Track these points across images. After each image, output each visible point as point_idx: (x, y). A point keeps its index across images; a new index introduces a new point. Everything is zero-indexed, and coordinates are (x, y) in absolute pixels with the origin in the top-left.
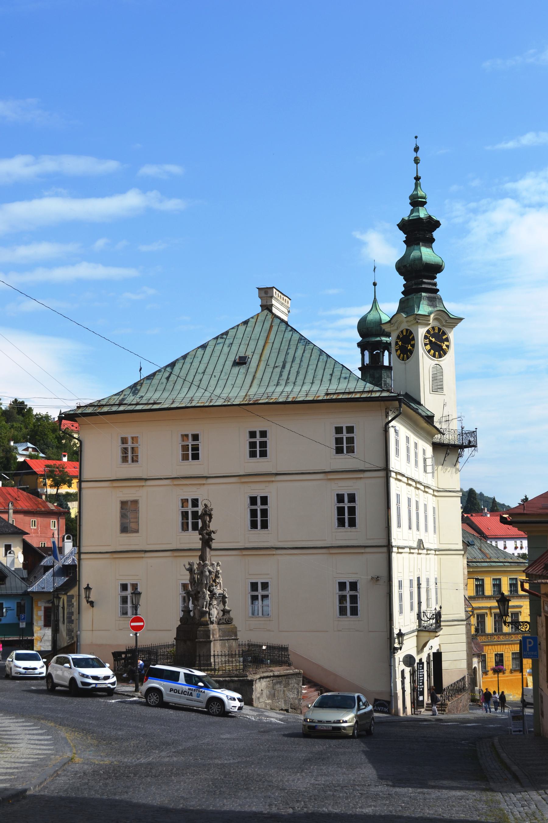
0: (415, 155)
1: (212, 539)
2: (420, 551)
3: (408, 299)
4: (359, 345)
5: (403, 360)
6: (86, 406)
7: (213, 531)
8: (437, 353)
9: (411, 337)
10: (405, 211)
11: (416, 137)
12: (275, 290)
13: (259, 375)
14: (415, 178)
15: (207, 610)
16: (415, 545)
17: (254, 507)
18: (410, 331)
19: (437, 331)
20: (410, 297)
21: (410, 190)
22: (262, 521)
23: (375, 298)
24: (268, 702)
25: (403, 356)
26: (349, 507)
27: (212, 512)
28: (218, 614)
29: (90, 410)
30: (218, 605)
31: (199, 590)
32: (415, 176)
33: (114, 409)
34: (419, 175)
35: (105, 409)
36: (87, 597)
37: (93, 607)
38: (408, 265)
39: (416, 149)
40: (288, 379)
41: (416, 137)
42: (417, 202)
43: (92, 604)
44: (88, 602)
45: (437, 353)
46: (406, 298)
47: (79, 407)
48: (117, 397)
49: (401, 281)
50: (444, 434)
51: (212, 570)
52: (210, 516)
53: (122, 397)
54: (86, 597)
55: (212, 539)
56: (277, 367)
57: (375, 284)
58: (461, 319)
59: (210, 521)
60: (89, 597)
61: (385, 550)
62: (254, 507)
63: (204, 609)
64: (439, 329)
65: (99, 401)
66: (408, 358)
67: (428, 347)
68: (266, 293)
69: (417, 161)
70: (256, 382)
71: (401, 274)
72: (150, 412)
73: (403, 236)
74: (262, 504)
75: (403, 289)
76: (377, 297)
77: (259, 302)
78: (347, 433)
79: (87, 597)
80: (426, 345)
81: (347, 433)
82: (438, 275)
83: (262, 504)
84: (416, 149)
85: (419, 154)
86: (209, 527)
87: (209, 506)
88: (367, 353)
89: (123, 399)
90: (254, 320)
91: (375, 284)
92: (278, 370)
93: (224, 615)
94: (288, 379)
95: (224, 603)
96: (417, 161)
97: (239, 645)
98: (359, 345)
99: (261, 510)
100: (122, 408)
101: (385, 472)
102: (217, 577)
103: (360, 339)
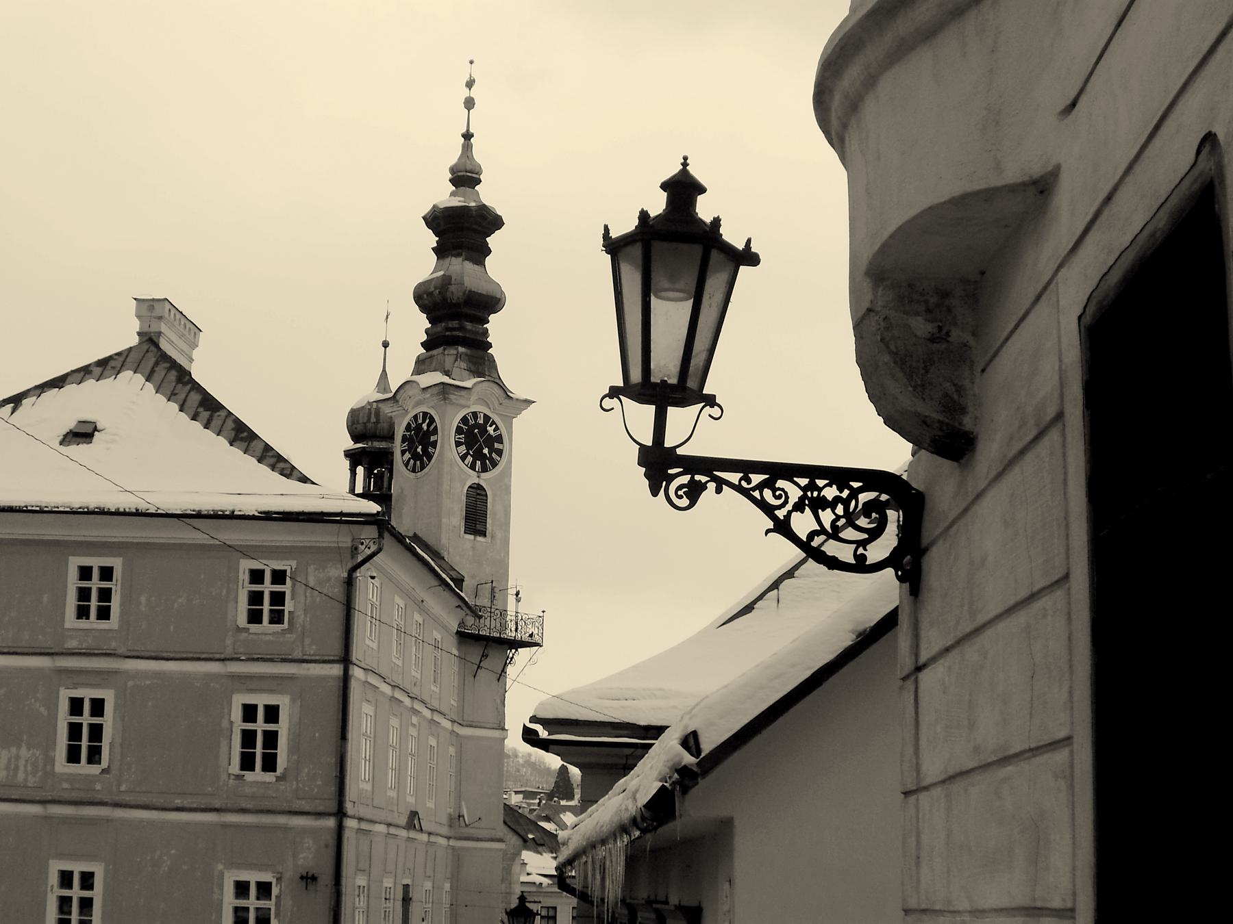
0: (466, 93)
2: (412, 834)
3: (431, 357)
4: (349, 454)
5: (414, 471)
8: (478, 463)
11: (471, 62)
12: (168, 306)
14: (463, 136)
16: (403, 820)
17: (76, 719)
20: (435, 352)
21: (453, 155)
22: (90, 748)
23: (384, 370)
25: (415, 464)
32: (464, 130)
39: (470, 84)
41: (471, 62)
42: (465, 178)
45: (478, 463)
49: (419, 324)
50: (480, 617)
58: (529, 402)
61: (331, 823)
62: (76, 719)
66: (423, 468)
67: (463, 449)
68: (151, 308)
69: (469, 104)
71: (423, 308)
73: (433, 240)
74: (267, 721)
75: (425, 337)
77: (136, 325)
78: (273, 583)
81: (273, 583)
82: (492, 317)
83: (267, 721)
84: (470, 84)
85: (474, 92)
88: (360, 470)
90: (122, 359)
98: (349, 454)
103: (350, 444)
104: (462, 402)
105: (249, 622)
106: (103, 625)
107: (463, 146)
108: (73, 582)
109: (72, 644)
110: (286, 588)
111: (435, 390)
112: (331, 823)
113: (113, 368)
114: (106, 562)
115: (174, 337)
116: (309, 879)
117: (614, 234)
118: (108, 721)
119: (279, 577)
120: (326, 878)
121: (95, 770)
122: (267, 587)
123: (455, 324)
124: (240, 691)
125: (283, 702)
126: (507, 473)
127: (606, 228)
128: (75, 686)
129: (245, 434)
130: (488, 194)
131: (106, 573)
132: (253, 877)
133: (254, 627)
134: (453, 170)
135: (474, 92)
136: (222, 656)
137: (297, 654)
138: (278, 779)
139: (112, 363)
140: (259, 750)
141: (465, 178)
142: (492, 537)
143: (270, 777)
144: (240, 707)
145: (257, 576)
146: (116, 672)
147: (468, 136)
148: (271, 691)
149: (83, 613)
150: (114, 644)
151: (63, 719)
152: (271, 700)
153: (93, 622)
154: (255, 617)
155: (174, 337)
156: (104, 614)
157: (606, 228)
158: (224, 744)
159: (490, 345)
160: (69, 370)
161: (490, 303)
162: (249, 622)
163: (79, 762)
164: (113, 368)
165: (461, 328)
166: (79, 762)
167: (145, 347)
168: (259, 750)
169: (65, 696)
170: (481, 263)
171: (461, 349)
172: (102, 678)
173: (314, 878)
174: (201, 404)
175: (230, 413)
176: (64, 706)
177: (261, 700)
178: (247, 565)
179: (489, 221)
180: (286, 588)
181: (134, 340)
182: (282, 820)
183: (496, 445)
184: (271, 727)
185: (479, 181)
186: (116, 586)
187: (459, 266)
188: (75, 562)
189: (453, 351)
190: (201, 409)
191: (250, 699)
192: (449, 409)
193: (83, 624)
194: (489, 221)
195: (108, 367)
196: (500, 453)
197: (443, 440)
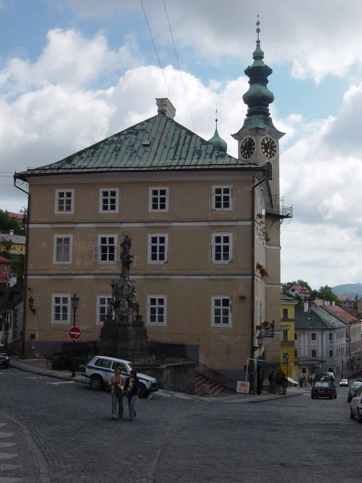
1: (130, 262)
3: (251, 119)
6: (35, 170)
7: (131, 256)
9: (252, 143)
10: (250, 62)
11: (258, 16)
13: (159, 153)
15: (126, 315)
18: (252, 139)
19: (269, 141)
21: (254, 49)
22: (160, 255)
24: (171, 385)
26: (224, 246)
27: (132, 242)
28: (133, 318)
29: (37, 172)
30: (133, 312)
31: (119, 300)
32: (257, 40)
33: (55, 171)
34: (260, 40)
35: (48, 172)
36: (31, 307)
37: (35, 313)
38: (252, 96)
39: (258, 24)
40: (180, 156)
42: (258, 56)
43: (34, 311)
44: (31, 310)
46: (249, 118)
47: (28, 170)
48: (56, 165)
49: (245, 108)
51: (130, 285)
52: (130, 245)
53: (59, 165)
54: (30, 306)
55: (130, 262)
56: (172, 148)
57: (216, 120)
59: (129, 248)
60: (32, 306)
63: (124, 314)
64: (271, 139)
65: (44, 167)
66: (249, 157)
69: (258, 31)
70: (157, 157)
72: (82, 175)
74: (160, 242)
76: (217, 129)
79: (31, 307)
80: (262, 148)
82: (270, 105)
83: (160, 242)
84: (258, 24)
85: (260, 27)
86: (128, 253)
87: (129, 237)
89: (61, 166)
91: (216, 120)
92: (173, 151)
93: (137, 319)
94: (180, 156)
95: (137, 311)
96: (258, 31)
97: (148, 342)
99: (160, 247)
100: (60, 171)
101: (252, 222)
102: (133, 290)
104: (262, 133)
105: (216, 208)
106: (163, 211)
107: (257, 45)
108: (151, 196)
109: (152, 218)
110: (229, 195)
111: (254, 130)
112: (250, 277)
113: (152, 122)
114: (163, 188)
115: (169, 112)
116: (242, 298)
117: (17, 173)
118: (166, 244)
119: (226, 191)
120: (248, 298)
121: (162, 262)
122: (222, 195)
123: (258, 107)
124: (100, 233)
125: (230, 235)
126: (278, 159)
127: (16, 172)
128: (154, 233)
129: (205, 143)
130: (267, 61)
131: (163, 192)
132: (221, 298)
133: (218, 209)
134: (254, 54)
135: (260, 27)
136: (207, 220)
137: (235, 218)
138: (229, 262)
139: (151, 121)
140: (222, 252)
141: (258, 56)
142: (274, 180)
143: (226, 262)
144: (100, 239)
145: (218, 191)
146: (118, 228)
147: (258, 42)
148: (226, 231)
149: (155, 207)
150: (167, 217)
151: (150, 244)
152: (226, 235)
153: (159, 210)
154: (218, 205)
155: (169, 112)
156: (163, 207)
157: (16, 172)
158: (210, 252)
159: (269, 114)
160: (136, 124)
161: (269, 99)
162: (216, 208)
163: (156, 259)
164: (152, 122)
165: (261, 108)
166: (156, 259)
167: (161, 115)
168: (222, 252)
169: (150, 236)
170: (266, 86)
171: (261, 116)
172: (115, 230)
173: (244, 298)
174: (186, 133)
175: (198, 136)
176: (150, 240)
177: (222, 235)
178: (215, 187)
179: (267, 71)
180: (229, 195)
181: (156, 113)
182: (232, 277)
183: (274, 149)
184: (162, 245)
185: (263, 57)
186: (167, 196)
187: (258, 87)
188: (151, 189)
189: (258, 116)
190: (187, 135)
191: (218, 235)
192: (259, 136)
193: (155, 211)
194: (267, 71)
195: (150, 122)
196: (275, 151)
197: (257, 147)
